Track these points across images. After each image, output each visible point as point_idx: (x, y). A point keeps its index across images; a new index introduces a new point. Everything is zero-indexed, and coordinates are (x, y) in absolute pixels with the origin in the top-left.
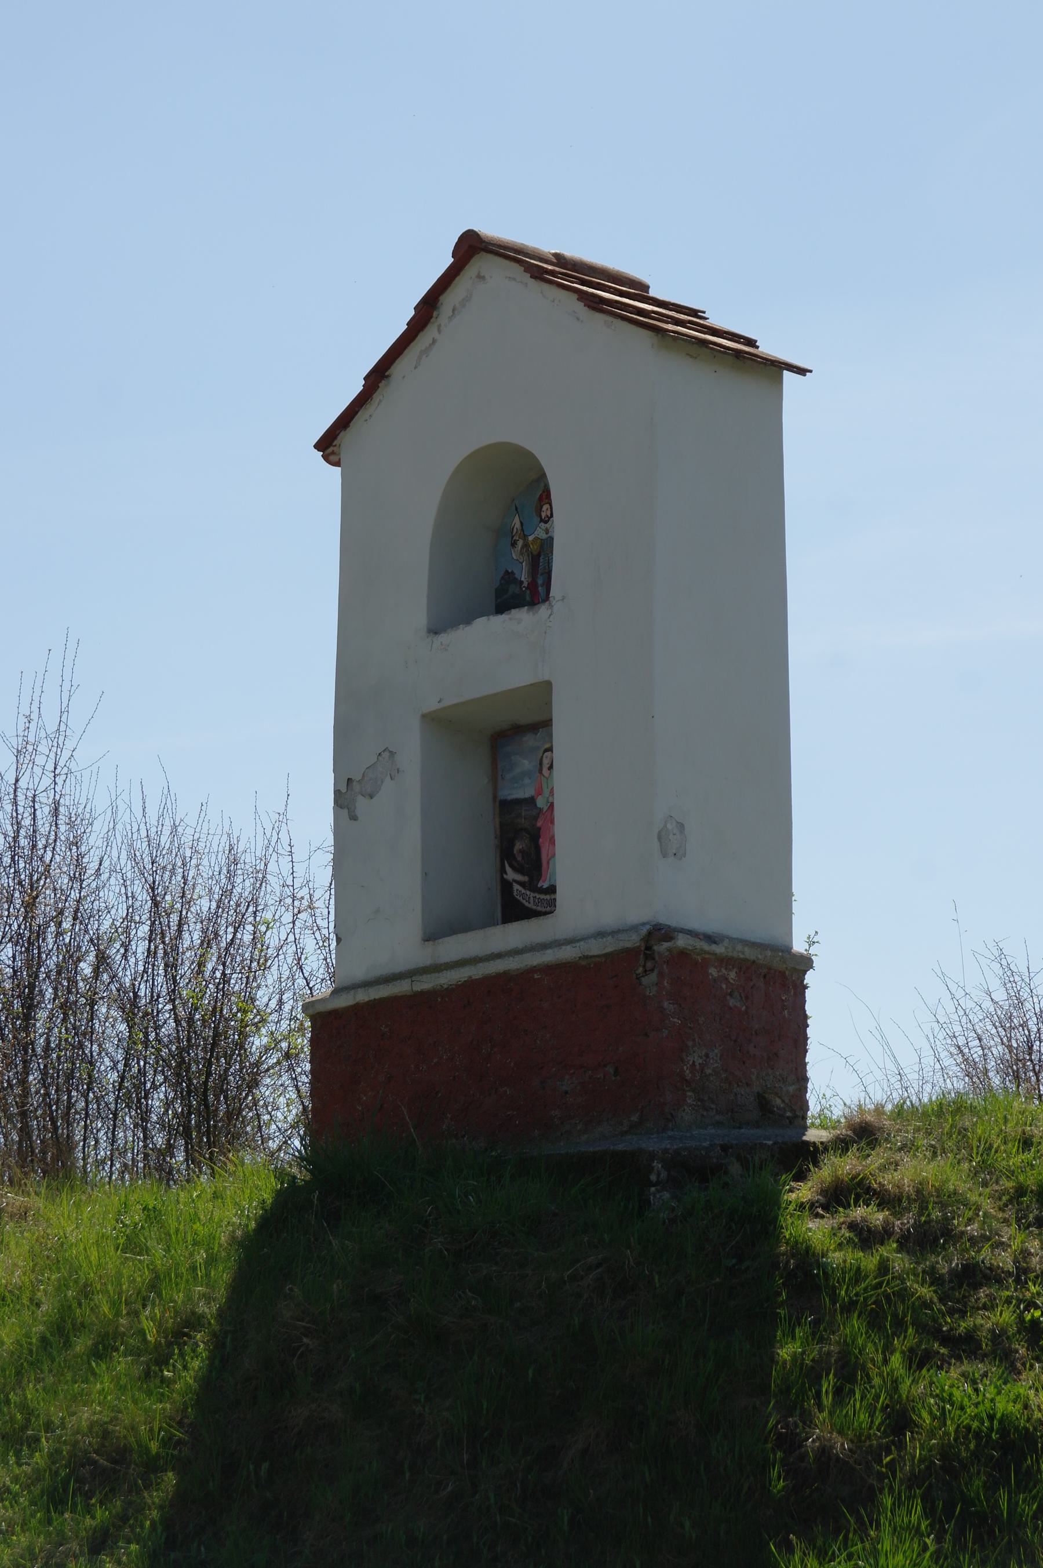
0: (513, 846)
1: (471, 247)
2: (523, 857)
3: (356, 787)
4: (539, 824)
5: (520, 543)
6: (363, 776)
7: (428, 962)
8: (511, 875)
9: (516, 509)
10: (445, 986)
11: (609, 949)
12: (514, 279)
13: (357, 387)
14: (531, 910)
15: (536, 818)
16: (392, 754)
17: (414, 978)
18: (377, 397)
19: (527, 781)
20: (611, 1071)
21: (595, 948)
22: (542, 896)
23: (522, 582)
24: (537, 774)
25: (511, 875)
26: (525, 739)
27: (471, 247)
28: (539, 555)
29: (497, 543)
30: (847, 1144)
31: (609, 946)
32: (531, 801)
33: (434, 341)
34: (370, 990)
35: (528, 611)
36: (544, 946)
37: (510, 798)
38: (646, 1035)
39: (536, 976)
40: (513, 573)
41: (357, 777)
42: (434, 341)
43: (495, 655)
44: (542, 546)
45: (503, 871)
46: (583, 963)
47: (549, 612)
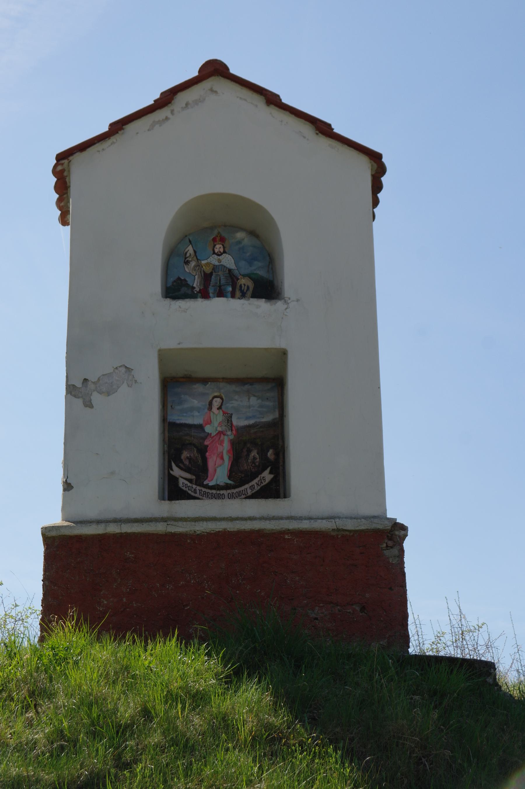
0: (181, 454)
1: (214, 70)
2: (190, 462)
3: (91, 386)
4: (206, 443)
5: (193, 264)
6: (99, 379)
7: (165, 515)
8: (176, 472)
9: (190, 242)
10: (198, 533)
11: (363, 528)
12: (245, 100)
13: (105, 128)
14: (192, 496)
15: (204, 439)
16: (128, 370)
17: (169, 523)
18: (113, 139)
19: (196, 414)
20: (358, 608)
21: (350, 525)
22: (210, 491)
23: (194, 288)
24: (206, 410)
25: (176, 472)
26: (195, 386)
27: (214, 70)
28: (211, 274)
29: (225, 254)
30: (194, 697)
31: (363, 526)
32: (200, 427)
33: (167, 119)
34: (123, 525)
35: (266, 302)
36: (274, 518)
37: (178, 422)
38: (391, 589)
39: (286, 537)
40: (185, 280)
41: (93, 378)
42: (167, 119)
43: (227, 325)
44: (213, 269)
45: (170, 467)
46: (333, 534)
47: (286, 306)
